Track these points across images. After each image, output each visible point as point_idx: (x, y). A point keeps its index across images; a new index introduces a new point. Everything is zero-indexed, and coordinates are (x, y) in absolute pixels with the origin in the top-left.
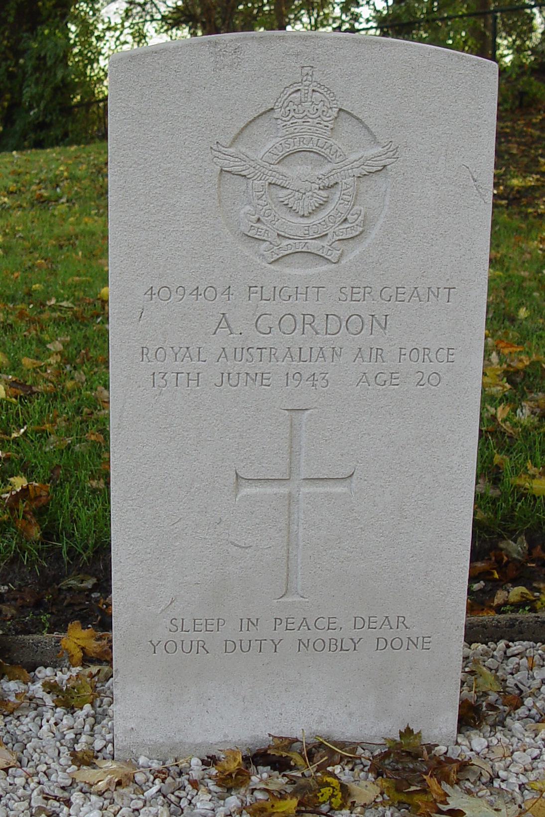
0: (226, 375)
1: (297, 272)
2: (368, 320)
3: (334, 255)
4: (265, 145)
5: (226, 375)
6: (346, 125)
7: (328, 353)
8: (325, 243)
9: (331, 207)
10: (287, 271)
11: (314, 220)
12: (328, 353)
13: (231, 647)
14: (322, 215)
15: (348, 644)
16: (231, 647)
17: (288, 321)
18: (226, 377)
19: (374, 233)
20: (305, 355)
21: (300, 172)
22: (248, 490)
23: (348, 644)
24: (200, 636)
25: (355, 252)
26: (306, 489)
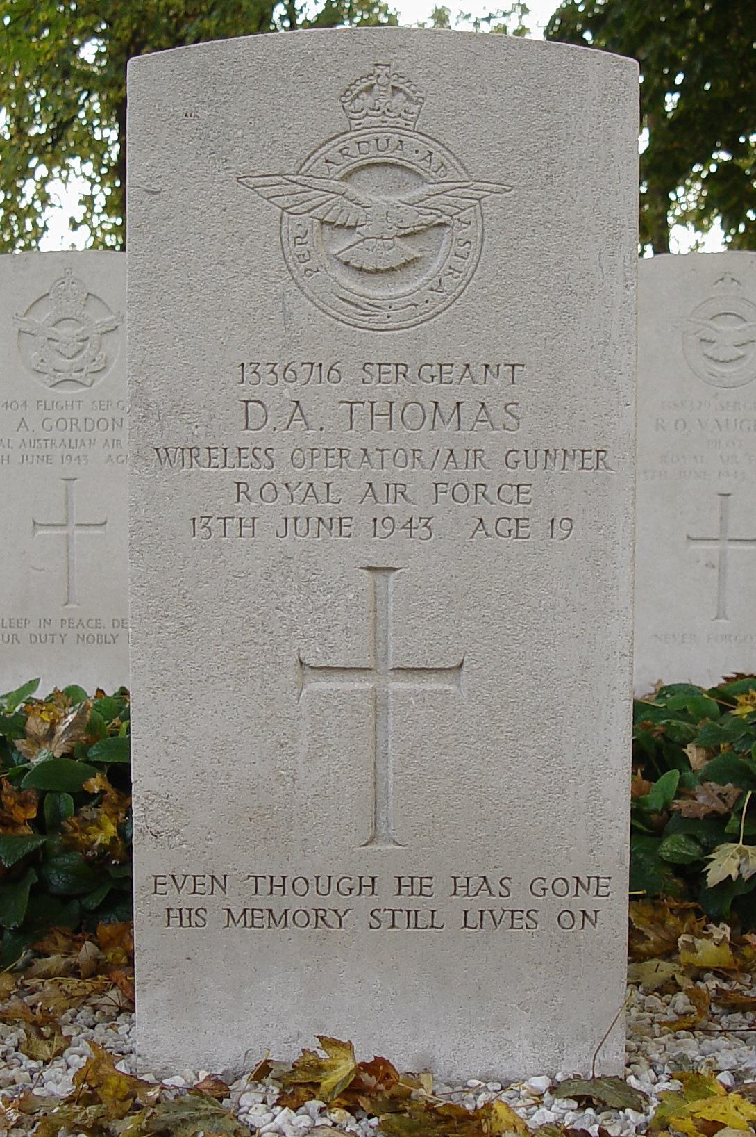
0: (413, 913)
1: (66, 392)
2: (110, 422)
3: (88, 382)
4: (45, 314)
5: (413, 913)
6: (92, 302)
7: (87, 442)
8: (83, 374)
9: (84, 352)
10: (405, 247)
11: (75, 360)
12: (87, 442)
13: (33, 639)
14: (81, 356)
15: (110, 639)
16: (33, 639)
17: (103, 424)
18: (25, 458)
19: (111, 369)
20: (73, 444)
21: (65, 331)
22: (41, 532)
23: (110, 639)
24: (14, 631)
25: (101, 379)
26: (79, 531)
